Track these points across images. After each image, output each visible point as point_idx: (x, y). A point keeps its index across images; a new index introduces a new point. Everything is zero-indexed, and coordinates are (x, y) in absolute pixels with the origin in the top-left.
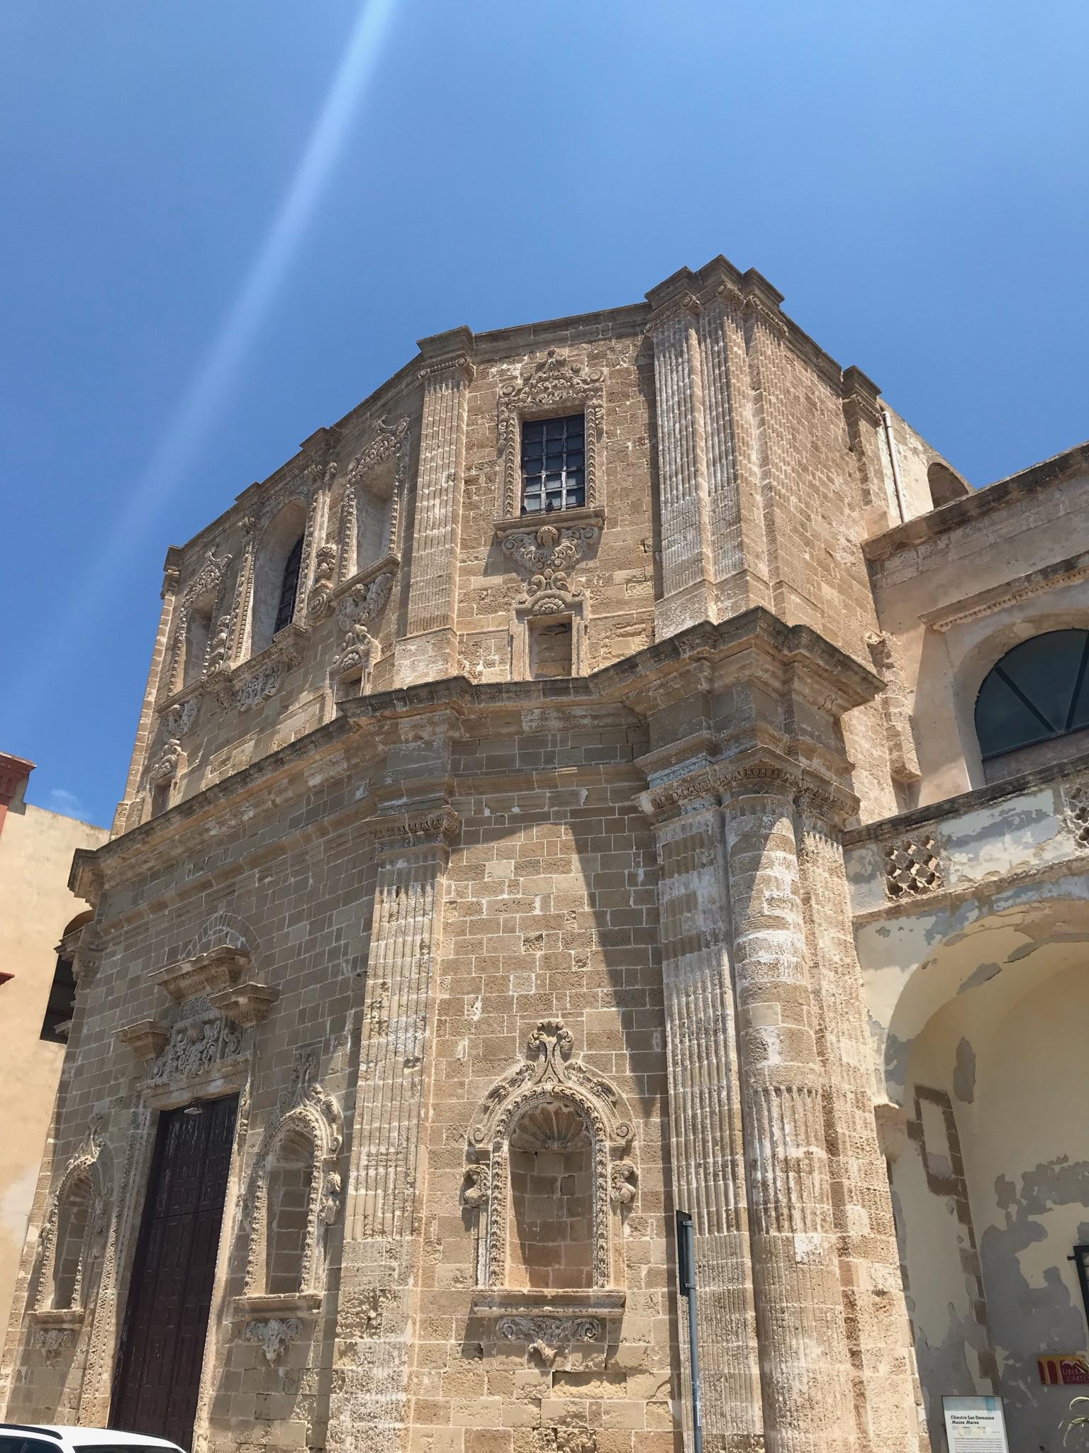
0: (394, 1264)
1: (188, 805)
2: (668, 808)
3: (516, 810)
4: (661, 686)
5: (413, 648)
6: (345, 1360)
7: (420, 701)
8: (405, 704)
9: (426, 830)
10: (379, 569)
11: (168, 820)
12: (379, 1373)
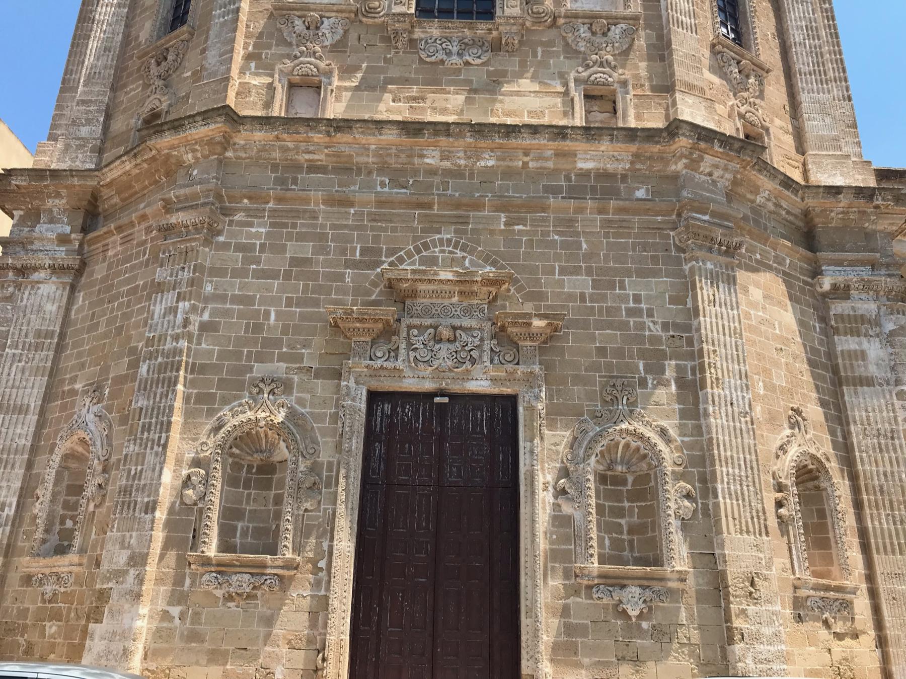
0: (761, 555)
1: (418, 126)
2: (841, 292)
3: (758, 256)
4: (843, 213)
5: (690, 101)
6: (740, 620)
7: (730, 149)
8: (720, 147)
9: (728, 247)
10: (625, 18)
11: (351, 128)
12: (767, 631)
